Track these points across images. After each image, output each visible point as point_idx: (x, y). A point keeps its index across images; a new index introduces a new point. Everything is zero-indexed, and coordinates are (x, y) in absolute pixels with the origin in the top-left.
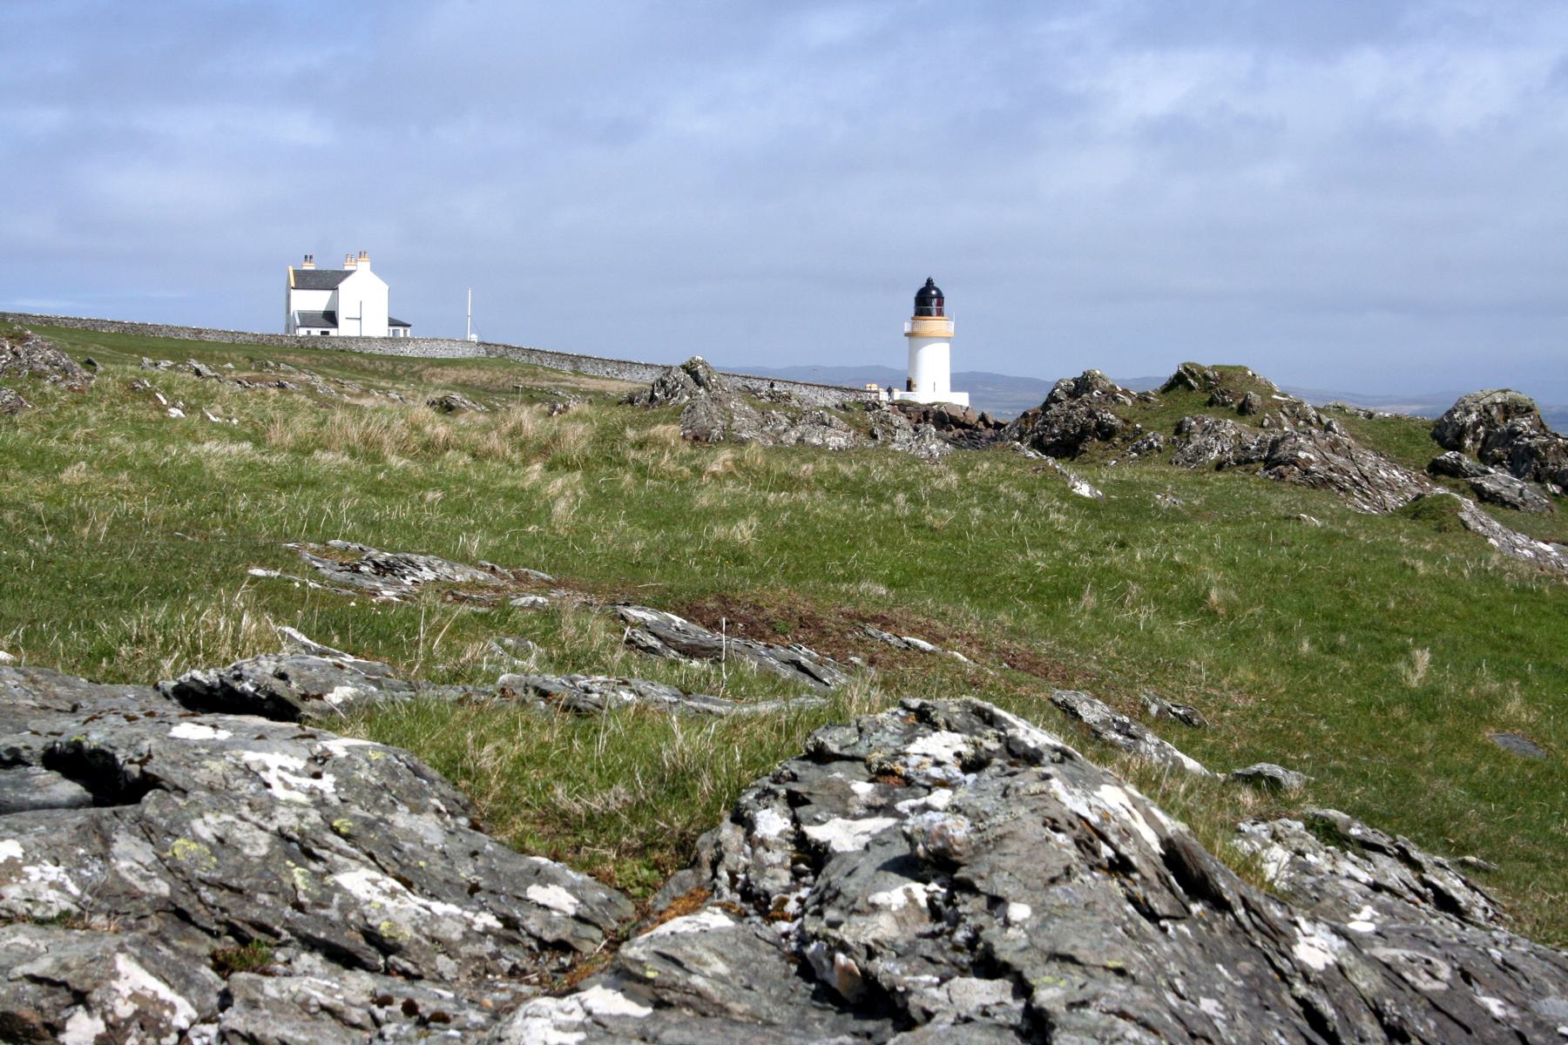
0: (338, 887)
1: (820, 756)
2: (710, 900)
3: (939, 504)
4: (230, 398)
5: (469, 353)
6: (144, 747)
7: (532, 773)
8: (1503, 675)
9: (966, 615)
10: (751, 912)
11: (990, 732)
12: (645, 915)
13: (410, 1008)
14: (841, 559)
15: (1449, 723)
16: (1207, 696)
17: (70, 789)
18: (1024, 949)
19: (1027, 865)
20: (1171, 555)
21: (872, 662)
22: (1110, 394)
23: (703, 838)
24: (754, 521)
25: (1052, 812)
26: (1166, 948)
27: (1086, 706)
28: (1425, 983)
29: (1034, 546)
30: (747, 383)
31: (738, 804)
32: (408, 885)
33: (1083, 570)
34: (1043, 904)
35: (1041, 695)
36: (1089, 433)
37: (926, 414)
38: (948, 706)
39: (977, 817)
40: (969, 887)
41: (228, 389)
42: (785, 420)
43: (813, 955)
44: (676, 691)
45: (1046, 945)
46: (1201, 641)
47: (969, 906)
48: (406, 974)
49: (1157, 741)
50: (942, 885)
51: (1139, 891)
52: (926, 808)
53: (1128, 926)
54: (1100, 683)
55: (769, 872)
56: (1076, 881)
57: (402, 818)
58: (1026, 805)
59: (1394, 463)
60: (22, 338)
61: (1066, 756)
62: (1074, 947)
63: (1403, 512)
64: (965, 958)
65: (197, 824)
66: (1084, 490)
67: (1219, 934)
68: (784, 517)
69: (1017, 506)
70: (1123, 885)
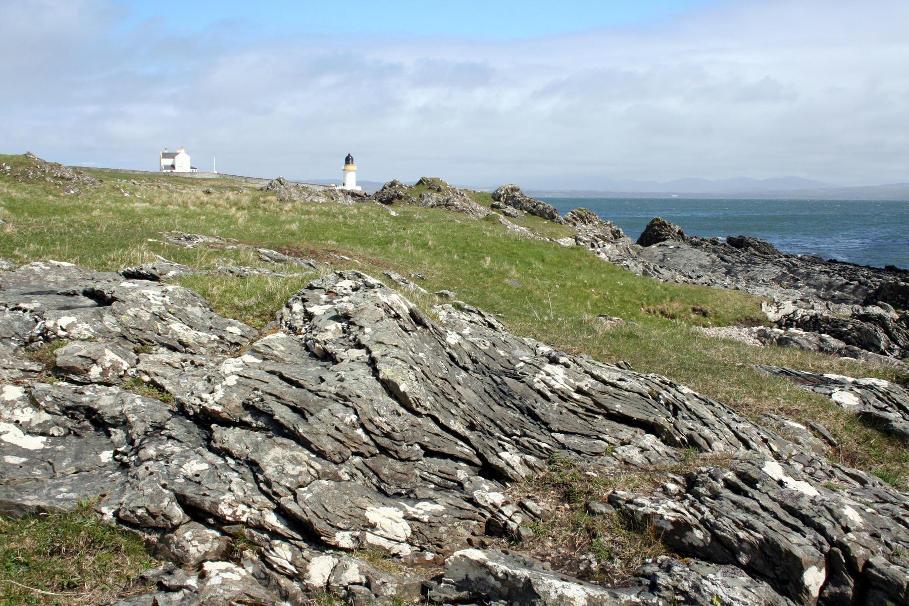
0: (170, 329)
1: (311, 288)
3: (351, 218)
4: (143, 188)
5: (214, 177)
6: (112, 289)
7: (228, 295)
8: (511, 264)
13: (192, 363)
15: (495, 278)
17: (91, 302)
22: (401, 186)
24: (297, 223)
28: (483, 347)
32: (191, 327)
38: (348, 273)
39: (356, 304)
40: (353, 324)
41: (142, 188)
47: (354, 329)
48: (191, 353)
51: (402, 324)
57: (189, 308)
59: (481, 205)
60: (80, 173)
61: (382, 286)
63: (484, 219)
64: (352, 344)
65: (128, 311)
66: (393, 214)
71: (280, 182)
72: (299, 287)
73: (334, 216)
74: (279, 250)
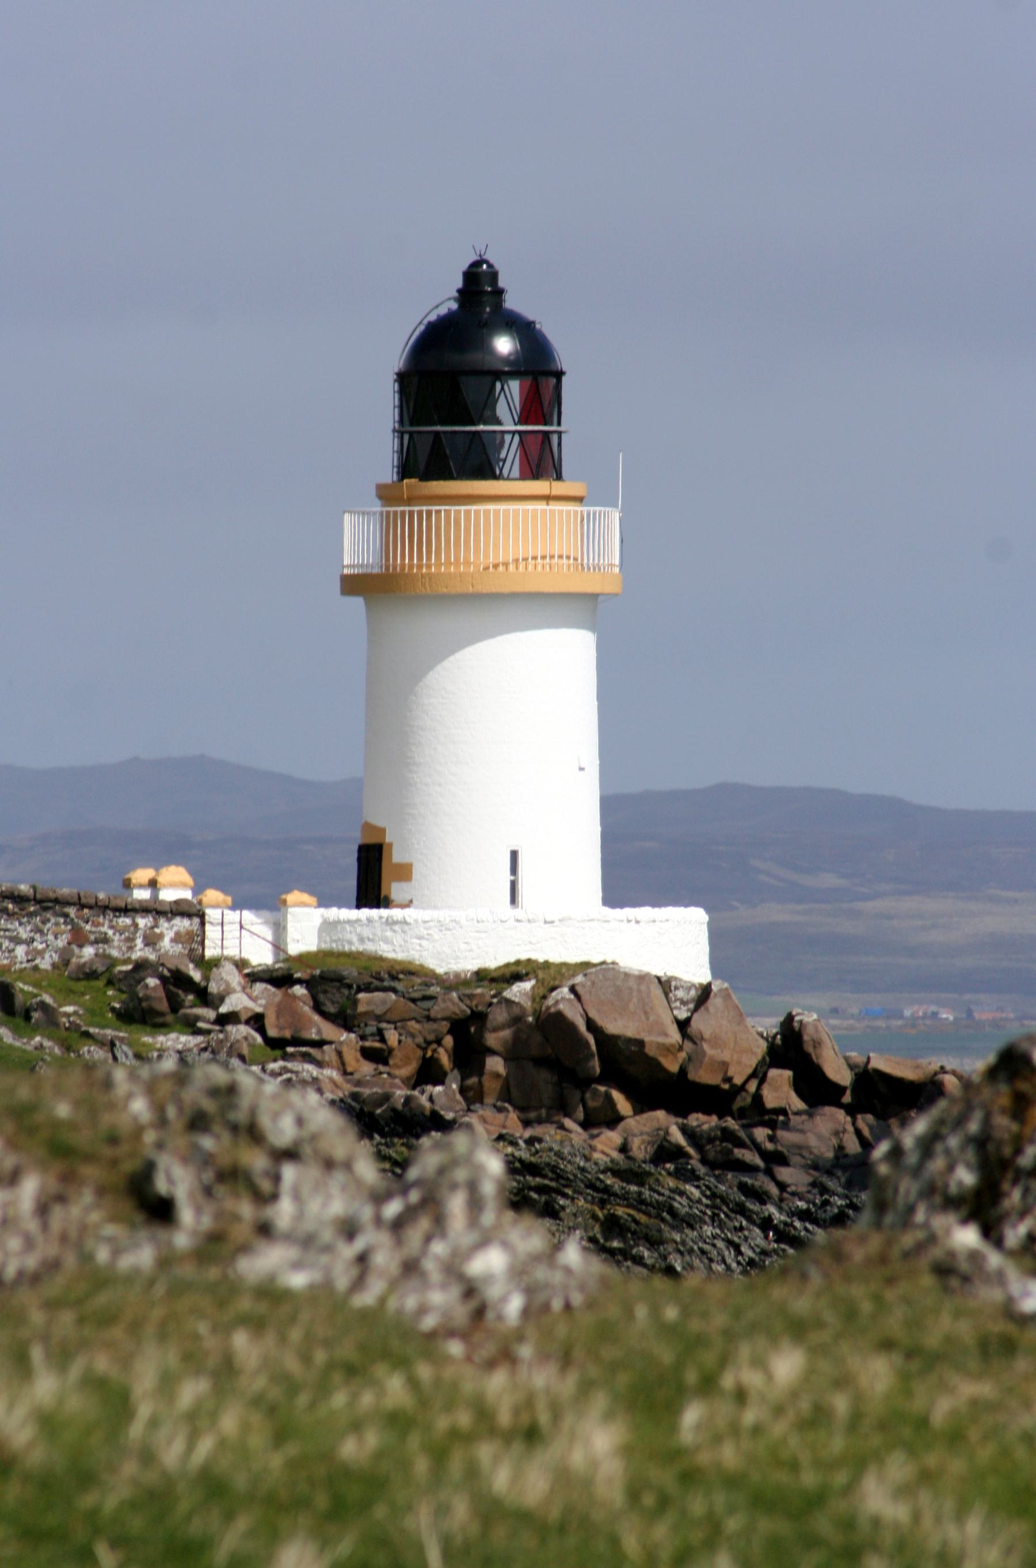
37: (467, 1034)
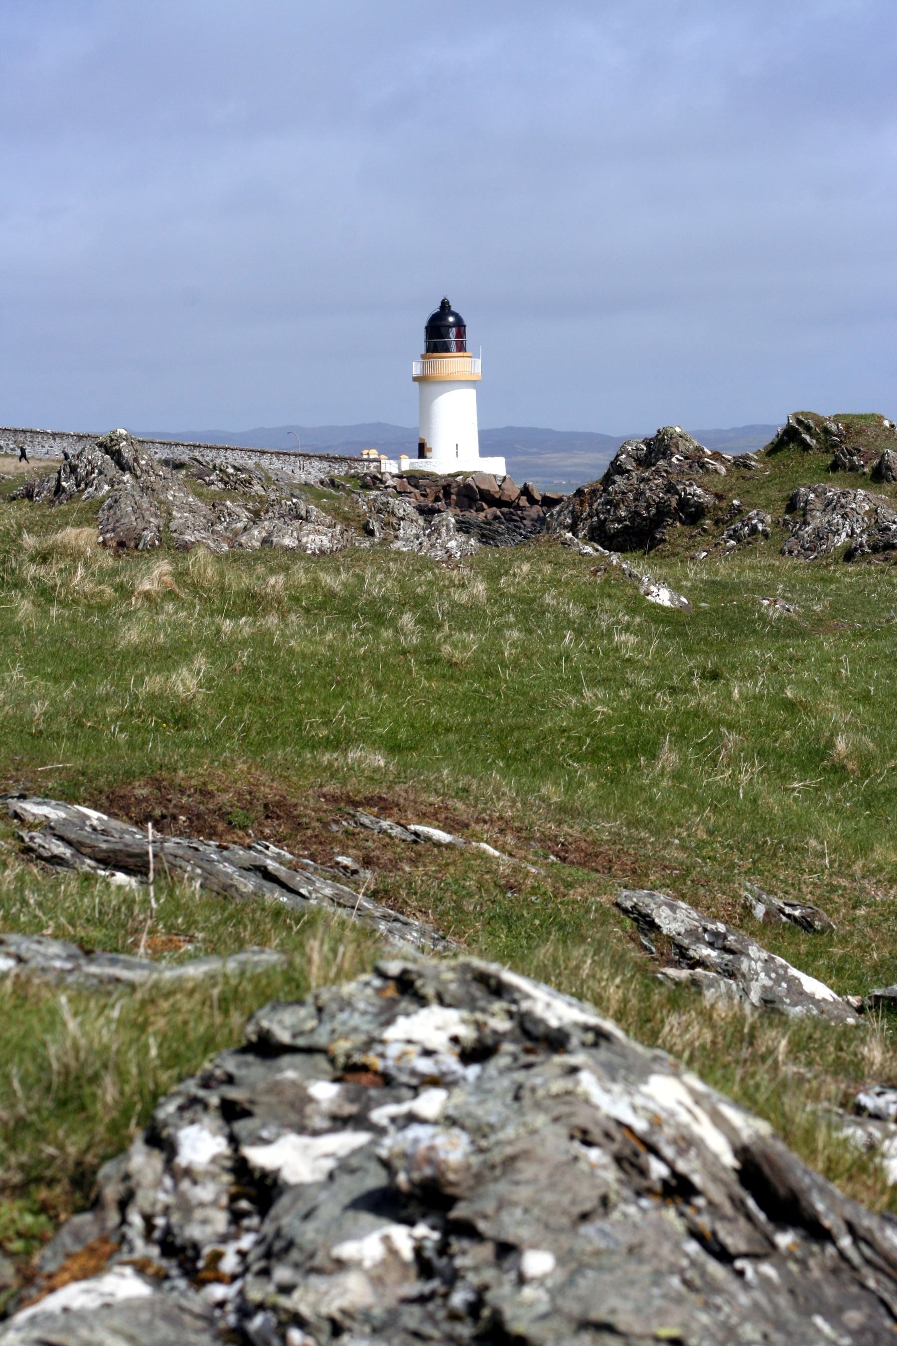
1: (266, 1048)
2: (117, 1258)
9: (496, 791)
10: (174, 1272)
11: (498, 1006)
12: (28, 1278)
14: (324, 713)
16: (833, 889)
18: (544, 1317)
19: (549, 1198)
20: (782, 689)
21: (367, 862)
22: (696, 460)
23: (107, 1169)
24: (201, 662)
25: (582, 1119)
26: (744, 1299)
27: (665, 911)
29: (595, 682)
30: (197, 454)
31: (153, 1119)
33: (660, 715)
34: (571, 1251)
35: (603, 899)
36: (668, 514)
37: (447, 489)
39: (479, 1131)
40: (467, 1230)
42: (245, 515)
43: (258, 1332)
44: (74, 949)
45: (573, 1308)
46: (824, 810)
47: (470, 1257)
49: (764, 955)
50: (433, 1228)
51: (704, 1222)
52: (412, 1118)
53: (690, 1274)
54: (684, 877)
55: (198, 1214)
56: (616, 1215)
58: (546, 1110)
61: (601, 1036)
62: (613, 1311)
66: (663, 597)
67: (816, 1273)
68: (244, 656)
69: (570, 624)
70: (681, 1215)
71: (117, 456)
72: (209, 1044)
73: (379, 619)
74: (113, 803)
